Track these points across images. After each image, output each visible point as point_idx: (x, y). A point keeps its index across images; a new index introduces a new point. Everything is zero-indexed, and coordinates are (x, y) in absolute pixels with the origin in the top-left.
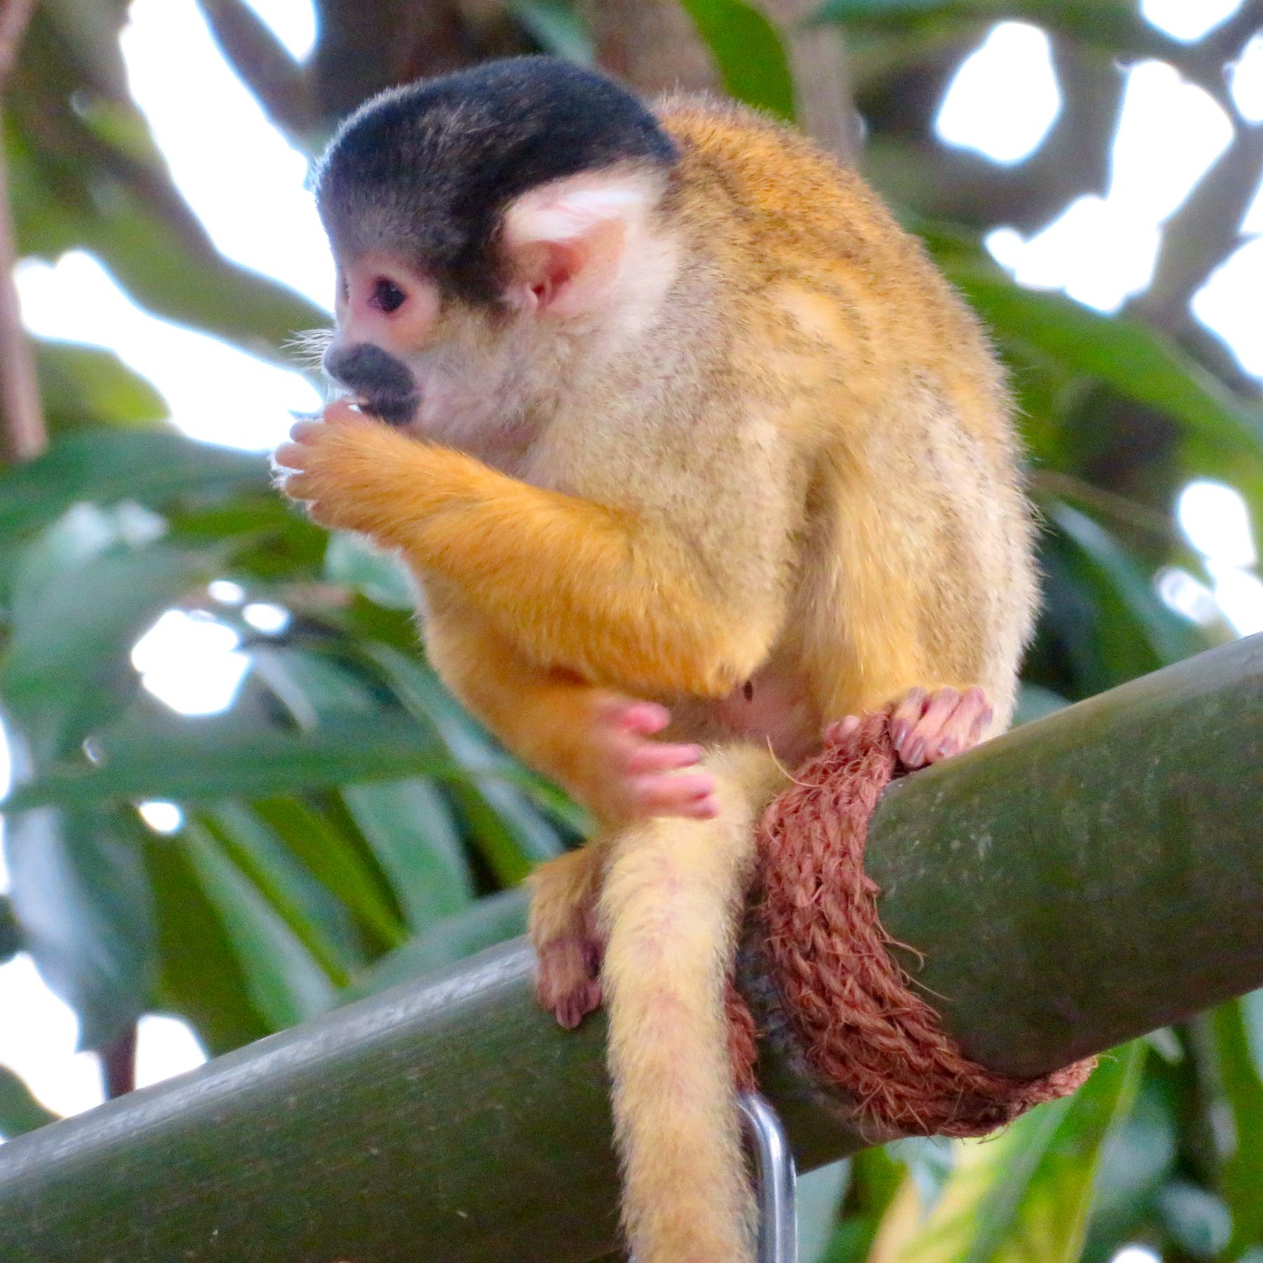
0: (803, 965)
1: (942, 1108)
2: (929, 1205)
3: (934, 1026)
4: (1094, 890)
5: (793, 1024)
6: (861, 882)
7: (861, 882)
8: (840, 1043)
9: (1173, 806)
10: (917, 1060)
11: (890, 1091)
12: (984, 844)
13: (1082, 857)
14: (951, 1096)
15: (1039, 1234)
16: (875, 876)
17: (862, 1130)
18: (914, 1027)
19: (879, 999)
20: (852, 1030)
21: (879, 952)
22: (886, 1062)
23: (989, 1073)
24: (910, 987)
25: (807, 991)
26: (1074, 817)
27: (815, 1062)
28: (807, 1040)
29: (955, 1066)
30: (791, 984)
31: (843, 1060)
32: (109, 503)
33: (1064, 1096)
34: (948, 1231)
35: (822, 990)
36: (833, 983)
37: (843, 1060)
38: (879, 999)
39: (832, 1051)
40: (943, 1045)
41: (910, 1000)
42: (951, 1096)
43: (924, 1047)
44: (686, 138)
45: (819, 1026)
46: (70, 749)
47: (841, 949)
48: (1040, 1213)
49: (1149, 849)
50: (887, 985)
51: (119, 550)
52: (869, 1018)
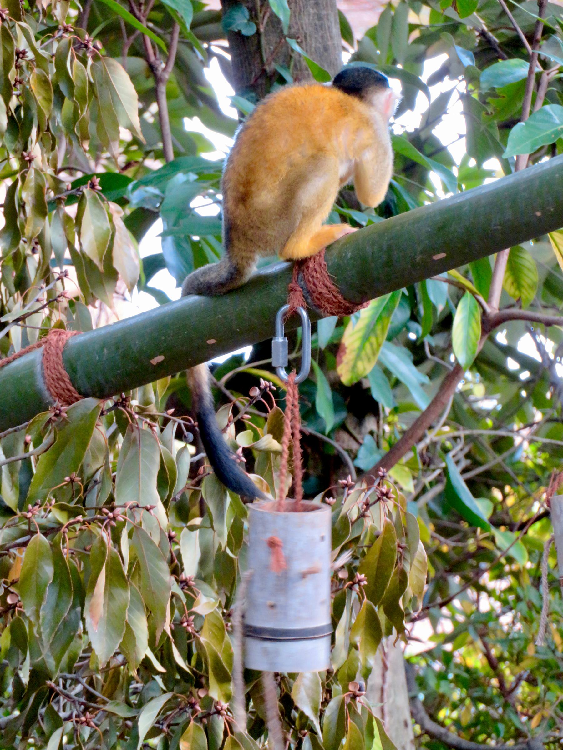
0: (311, 279)
1: (340, 310)
2: (354, 325)
3: (338, 292)
4: (373, 265)
5: (309, 292)
6: (324, 263)
7: (324, 263)
8: (319, 296)
9: (390, 248)
10: (335, 300)
11: (328, 306)
12: (349, 255)
13: (370, 258)
14: (341, 308)
15: (379, 332)
16: (325, 261)
17: (323, 314)
18: (334, 293)
19: (327, 287)
20: (320, 293)
21: (327, 277)
22: (328, 300)
23: (350, 302)
24: (334, 285)
25: (311, 285)
26: (368, 249)
27: (313, 300)
28: (311, 295)
29: (343, 301)
30: (308, 283)
31: (319, 299)
32: (186, 173)
33: (536, 260)
34: (359, 331)
35: (315, 285)
36: (317, 283)
37: (319, 299)
38: (327, 287)
39: (317, 298)
40: (340, 297)
41: (333, 287)
42: (341, 308)
43: (336, 297)
44: (38, 237)
45: (314, 292)
46: (176, 223)
47: (319, 276)
48: (379, 327)
49: (385, 257)
50: (328, 284)
51: (187, 182)
52: (324, 291)
